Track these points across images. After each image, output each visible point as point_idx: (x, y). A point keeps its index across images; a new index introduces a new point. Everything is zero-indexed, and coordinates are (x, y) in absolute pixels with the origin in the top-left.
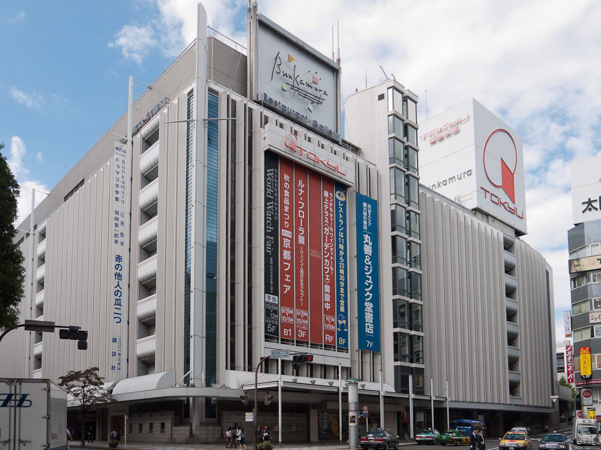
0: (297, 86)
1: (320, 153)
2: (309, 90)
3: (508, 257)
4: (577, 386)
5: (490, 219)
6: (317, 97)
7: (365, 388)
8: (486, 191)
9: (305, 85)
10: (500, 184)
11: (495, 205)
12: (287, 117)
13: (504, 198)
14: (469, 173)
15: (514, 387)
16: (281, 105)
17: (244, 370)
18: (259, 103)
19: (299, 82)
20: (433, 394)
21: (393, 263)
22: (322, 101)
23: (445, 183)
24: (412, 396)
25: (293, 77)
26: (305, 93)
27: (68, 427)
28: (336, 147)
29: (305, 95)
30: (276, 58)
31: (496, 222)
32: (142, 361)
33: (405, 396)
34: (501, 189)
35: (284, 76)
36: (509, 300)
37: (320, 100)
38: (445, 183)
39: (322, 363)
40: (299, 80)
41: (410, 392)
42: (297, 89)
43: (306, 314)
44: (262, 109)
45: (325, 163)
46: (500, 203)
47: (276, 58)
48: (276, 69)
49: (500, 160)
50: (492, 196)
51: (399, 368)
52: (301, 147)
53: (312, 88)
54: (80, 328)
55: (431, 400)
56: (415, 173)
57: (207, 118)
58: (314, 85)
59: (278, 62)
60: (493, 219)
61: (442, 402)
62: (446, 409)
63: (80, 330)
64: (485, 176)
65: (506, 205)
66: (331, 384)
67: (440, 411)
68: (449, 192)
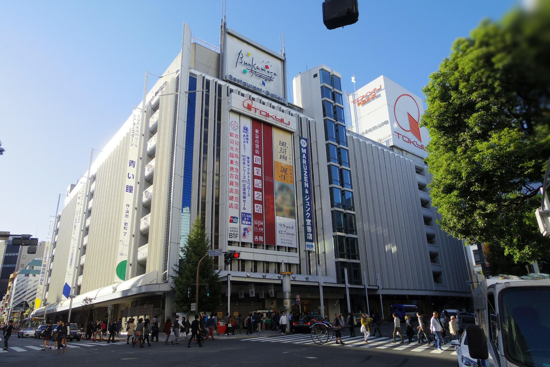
0: (255, 71)
1: (271, 112)
2: (263, 73)
3: (420, 178)
4: (301, 299)
5: (404, 152)
6: (269, 77)
7: (309, 280)
8: (398, 134)
9: (261, 69)
10: (409, 129)
11: (407, 143)
12: (247, 89)
13: (413, 138)
14: (386, 123)
15: (437, 276)
16: (242, 82)
17: (239, 270)
18: (226, 81)
19: (256, 68)
20: (366, 284)
21: (473, 250)
22: (273, 79)
23: (370, 130)
24: (348, 285)
25: (251, 65)
26: (260, 74)
27: (533, 266)
28: (283, 108)
29: (261, 75)
30: (239, 54)
31: (409, 154)
32: (140, 265)
33: (343, 286)
34: (410, 132)
35: (245, 64)
36: (425, 210)
37: (271, 79)
38: (370, 130)
39: (264, 260)
40: (255, 66)
41: (346, 282)
42: (254, 72)
43: (262, 223)
44: (228, 84)
45: (274, 117)
46: (410, 142)
47: (239, 54)
48: (240, 60)
49: (407, 114)
50: (404, 137)
51: (339, 263)
52: (256, 108)
53: (265, 71)
54: (32, 236)
55: (365, 288)
56: (342, 123)
57: (188, 91)
58: (267, 70)
59: (241, 56)
60: (407, 153)
61: (376, 290)
62: (379, 295)
63: (31, 237)
64: (402, 130)
65: (415, 143)
66: (264, 278)
67: (374, 297)
68: (374, 136)
